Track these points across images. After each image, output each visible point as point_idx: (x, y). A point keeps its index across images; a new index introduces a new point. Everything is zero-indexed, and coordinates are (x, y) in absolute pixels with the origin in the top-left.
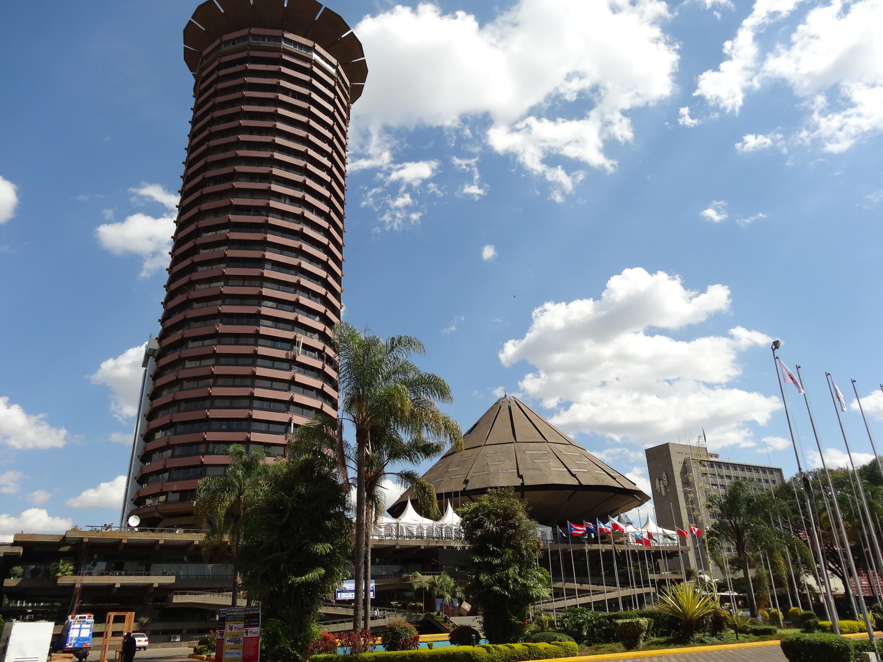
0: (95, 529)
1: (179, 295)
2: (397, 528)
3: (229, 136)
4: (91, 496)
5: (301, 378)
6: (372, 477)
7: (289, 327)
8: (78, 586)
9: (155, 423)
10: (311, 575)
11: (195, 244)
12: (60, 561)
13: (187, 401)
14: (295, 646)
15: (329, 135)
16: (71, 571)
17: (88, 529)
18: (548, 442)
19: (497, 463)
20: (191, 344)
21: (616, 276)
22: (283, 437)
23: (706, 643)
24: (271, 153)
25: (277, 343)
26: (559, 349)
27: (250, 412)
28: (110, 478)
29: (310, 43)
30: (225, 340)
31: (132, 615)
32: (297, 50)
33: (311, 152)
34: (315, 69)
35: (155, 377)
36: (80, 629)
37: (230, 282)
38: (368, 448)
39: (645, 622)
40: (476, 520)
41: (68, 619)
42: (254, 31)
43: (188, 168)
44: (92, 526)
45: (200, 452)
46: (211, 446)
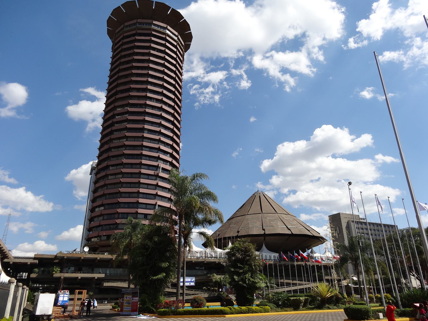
0: (69, 252)
1: (106, 145)
2: (205, 253)
3: (128, 71)
4: (66, 234)
5: (161, 184)
6: (186, 234)
7: (156, 160)
8: (62, 278)
9: (96, 204)
10: (159, 276)
11: (113, 113)
12: (54, 266)
13: (110, 194)
14: (153, 306)
15: (174, 69)
16: (59, 271)
17: (66, 253)
18: (277, 213)
19: (253, 223)
20: (115, 133)
21: (318, 129)
22: (153, 211)
23: (331, 308)
24: (147, 78)
25: (150, 167)
26: (289, 165)
27: (138, 199)
28: (74, 226)
29: (165, 26)
30: (126, 166)
31: (85, 291)
32: (159, 29)
33: (166, 78)
34: (168, 38)
35: (95, 183)
36: (64, 297)
37: (129, 139)
38: (183, 222)
39: (303, 299)
40: (233, 252)
41: (58, 292)
42: (139, 20)
43: (109, 86)
44: (68, 251)
45: (115, 217)
46: (120, 215)
